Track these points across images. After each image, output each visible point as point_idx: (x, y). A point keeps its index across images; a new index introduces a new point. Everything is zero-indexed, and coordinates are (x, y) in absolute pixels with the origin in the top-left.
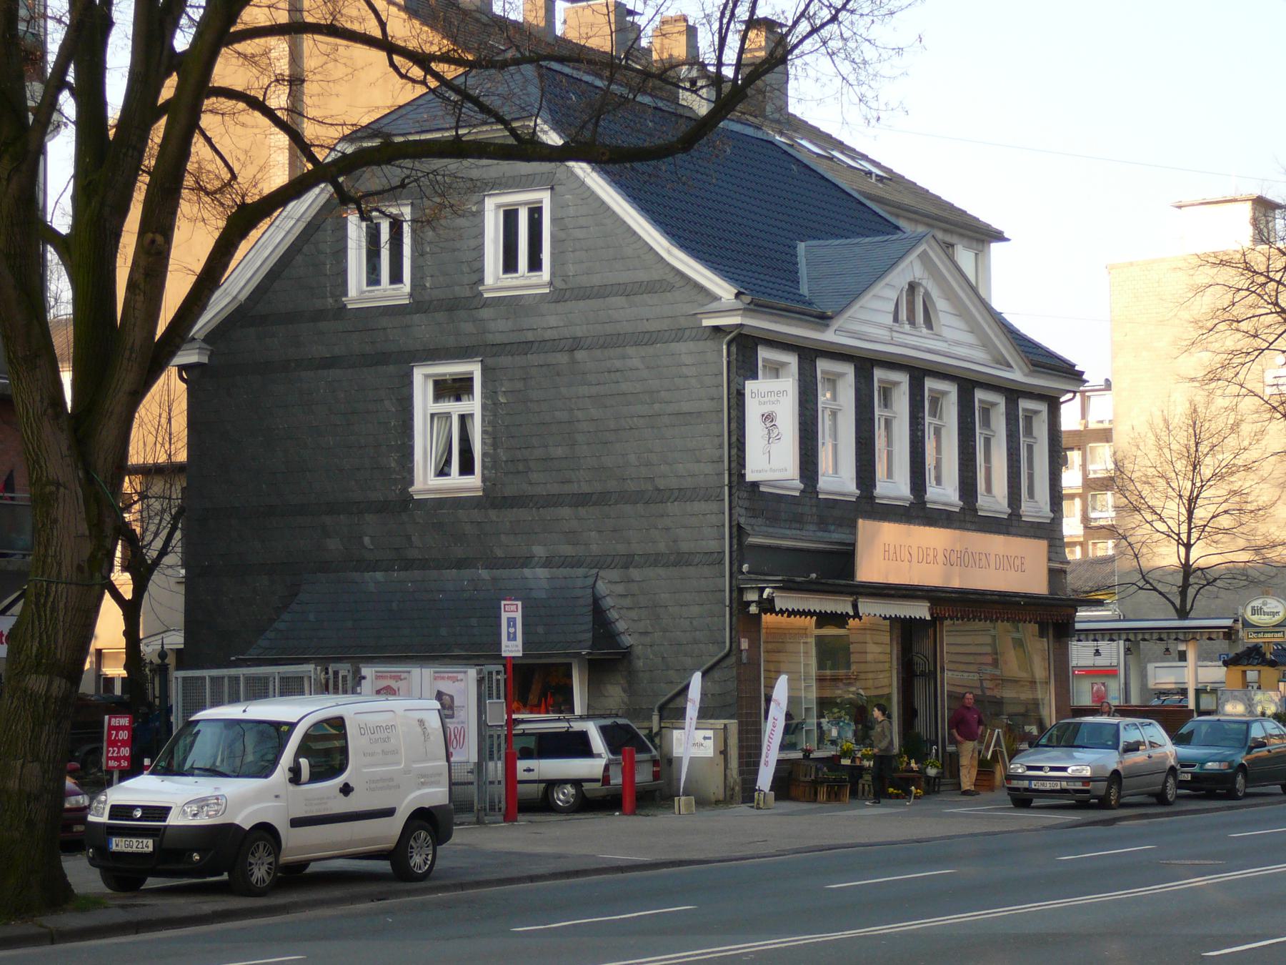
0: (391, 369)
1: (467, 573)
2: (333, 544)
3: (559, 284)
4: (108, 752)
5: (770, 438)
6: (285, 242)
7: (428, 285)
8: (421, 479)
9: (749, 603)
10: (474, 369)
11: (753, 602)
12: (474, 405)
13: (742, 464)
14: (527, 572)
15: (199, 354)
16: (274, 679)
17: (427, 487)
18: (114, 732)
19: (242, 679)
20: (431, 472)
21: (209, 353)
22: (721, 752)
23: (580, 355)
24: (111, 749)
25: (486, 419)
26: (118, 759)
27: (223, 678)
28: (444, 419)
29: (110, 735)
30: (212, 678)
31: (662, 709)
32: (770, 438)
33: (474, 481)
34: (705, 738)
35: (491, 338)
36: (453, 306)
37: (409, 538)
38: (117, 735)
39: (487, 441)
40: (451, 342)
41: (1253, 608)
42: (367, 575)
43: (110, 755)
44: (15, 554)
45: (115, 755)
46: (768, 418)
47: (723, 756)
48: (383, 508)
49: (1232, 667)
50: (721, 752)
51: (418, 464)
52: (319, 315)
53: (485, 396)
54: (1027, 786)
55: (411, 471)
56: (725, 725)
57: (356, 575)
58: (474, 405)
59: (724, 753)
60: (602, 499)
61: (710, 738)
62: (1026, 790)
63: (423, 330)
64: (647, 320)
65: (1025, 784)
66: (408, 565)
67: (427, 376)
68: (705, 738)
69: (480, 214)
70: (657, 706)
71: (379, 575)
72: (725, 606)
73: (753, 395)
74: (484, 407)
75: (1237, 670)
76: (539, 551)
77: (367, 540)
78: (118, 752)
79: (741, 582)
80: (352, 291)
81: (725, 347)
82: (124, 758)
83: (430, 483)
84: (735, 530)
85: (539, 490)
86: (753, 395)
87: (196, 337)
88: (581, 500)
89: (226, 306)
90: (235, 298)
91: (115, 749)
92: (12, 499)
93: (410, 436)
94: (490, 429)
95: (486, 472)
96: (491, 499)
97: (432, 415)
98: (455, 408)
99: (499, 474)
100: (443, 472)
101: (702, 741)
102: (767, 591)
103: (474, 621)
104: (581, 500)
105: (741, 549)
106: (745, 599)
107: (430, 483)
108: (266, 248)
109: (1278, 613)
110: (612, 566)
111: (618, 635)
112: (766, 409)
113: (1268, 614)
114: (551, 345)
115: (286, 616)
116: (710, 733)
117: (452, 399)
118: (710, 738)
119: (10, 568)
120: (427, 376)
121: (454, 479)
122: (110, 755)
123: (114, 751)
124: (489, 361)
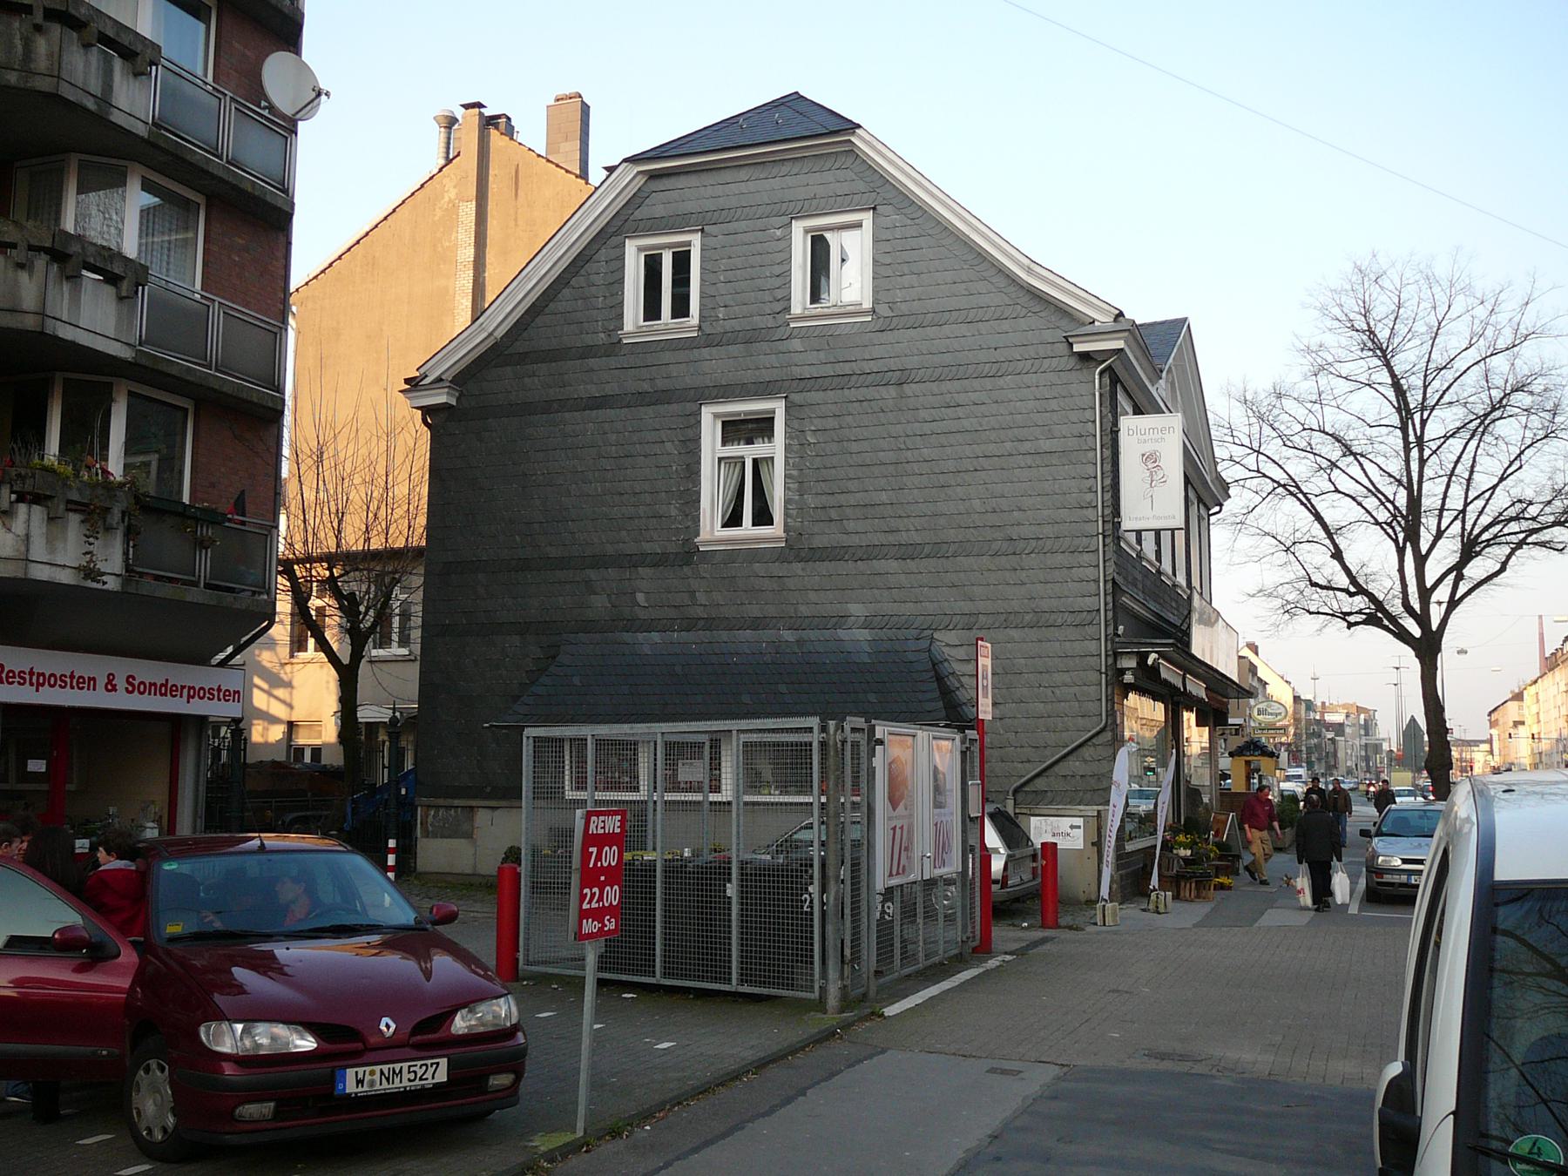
0: (674, 408)
1: (768, 635)
2: (599, 602)
3: (883, 310)
4: (583, 897)
5: (1152, 481)
6: (552, 272)
7: (721, 316)
8: (708, 528)
9: (1122, 672)
10: (778, 408)
11: (1129, 669)
12: (776, 448)
13: (1117, 512)
14: (841, 633)
15: (448, 393)
16: (655, 744)
17: (713, 538)
18: (594, 850)
19: (589, 742)
20: (720, 525)
21: (457, 394)
22: (1093, 844)
23: (908, 389)
24: (586, 891)
25: (791, 461)
26: (597, 914)
27: (561, 740)
28: (732, 465)
29: (586, 856)
30: (600, 743)
31: (1016, 791)
32: (1152, 481)
33: (776, 530)
34: (1072, 827)
35: (797, 372)
36: (751, 337)
37: (692, 593)
38: (599, 858)
39: (791, 485)
40: (749, 376)
41: (1259, 710)
42: (641, 636)
43: (585, 906)
44: (244, 590)
45: (594, 905)
46: (1151, 459)
47: (1096, 848)
48: (661, 561)
49: (1236, 758)
50: (1093, 844)
51: (704, 512)
52: (588, 352)
53: (788, 435)
54: (1405, 881)
55: (697, 520)
56: (1099, 812)
57: (627, 637)
58: (776, 448)
59: (1098, 845)
60: (938, 550)
61: (1079, 827)
62: (1402, 885)
63: (716, 364)
64: (995, 349)
65: (1404, 878)
66: (690, 624)
67: (716, 416)
68: (1072, 827)
69: (787, 238)
70: (1012, 788)
71: (655, 637)
72: (1101, 673)
73: (1131, 432)
74: (788, 448)
75: (1241, 761)
76: (856, 609)
77: (640, 597)
78: (601, 899)
79: (1118, 645)
80: (629, 326)
81: (1097, 377)
82: (611, 910)
83: (716, 534)
84: (1110, 585)
85: (855, 540)
86: (1131, 432)
87: (443, 377)
88: (908, 552)
89: (481, 342)
90: (491, 334)
91: (596, 890)
92: (243, 523)
93: (698, 483)
94: (795, 473)
95: (789, 520)
96: (796, 549)
97: (720, 460)
98: (749, 452)
99: (806, 523)
100: (734, 520)
101: (1069, 831)
102: (1153, 656)
103: (783, 688)
104: (908, 552)
105: (1118, 611)
106: (1119, 666)
107: (716, 534)
108: (530, 280)
109: (1280, 714)
110: (951, 627)
111: (960, 705)
112: (1148, 448)
113: (1272, 714)
114: (881, 379)
115: (544, 680)
116: (1079, 821)
117: (742, 442)
118: (1079, 827)
119: (237, 606)
120: (716, 416)
121: (746, 529)
122: (585, 906)
123: (593, 895)
124: (796, 398)
